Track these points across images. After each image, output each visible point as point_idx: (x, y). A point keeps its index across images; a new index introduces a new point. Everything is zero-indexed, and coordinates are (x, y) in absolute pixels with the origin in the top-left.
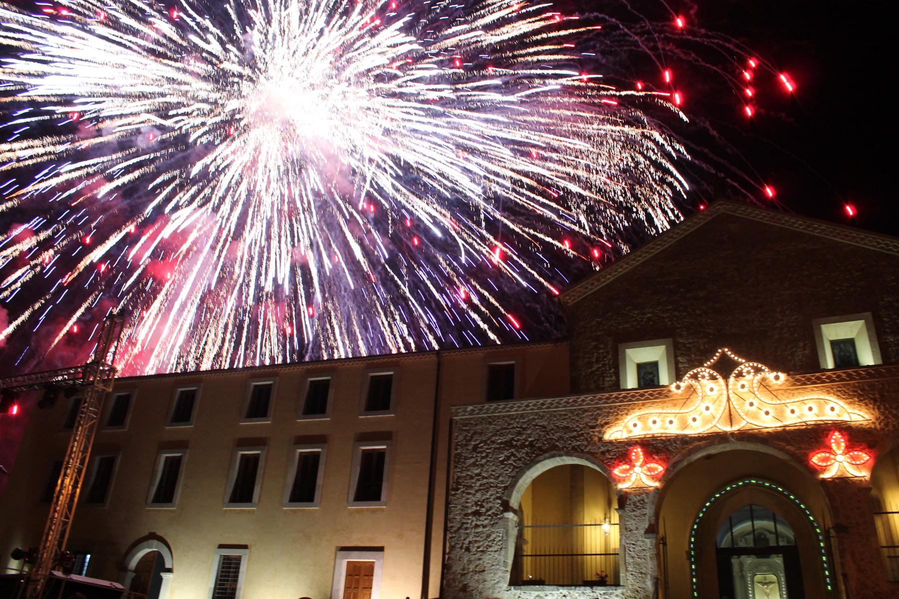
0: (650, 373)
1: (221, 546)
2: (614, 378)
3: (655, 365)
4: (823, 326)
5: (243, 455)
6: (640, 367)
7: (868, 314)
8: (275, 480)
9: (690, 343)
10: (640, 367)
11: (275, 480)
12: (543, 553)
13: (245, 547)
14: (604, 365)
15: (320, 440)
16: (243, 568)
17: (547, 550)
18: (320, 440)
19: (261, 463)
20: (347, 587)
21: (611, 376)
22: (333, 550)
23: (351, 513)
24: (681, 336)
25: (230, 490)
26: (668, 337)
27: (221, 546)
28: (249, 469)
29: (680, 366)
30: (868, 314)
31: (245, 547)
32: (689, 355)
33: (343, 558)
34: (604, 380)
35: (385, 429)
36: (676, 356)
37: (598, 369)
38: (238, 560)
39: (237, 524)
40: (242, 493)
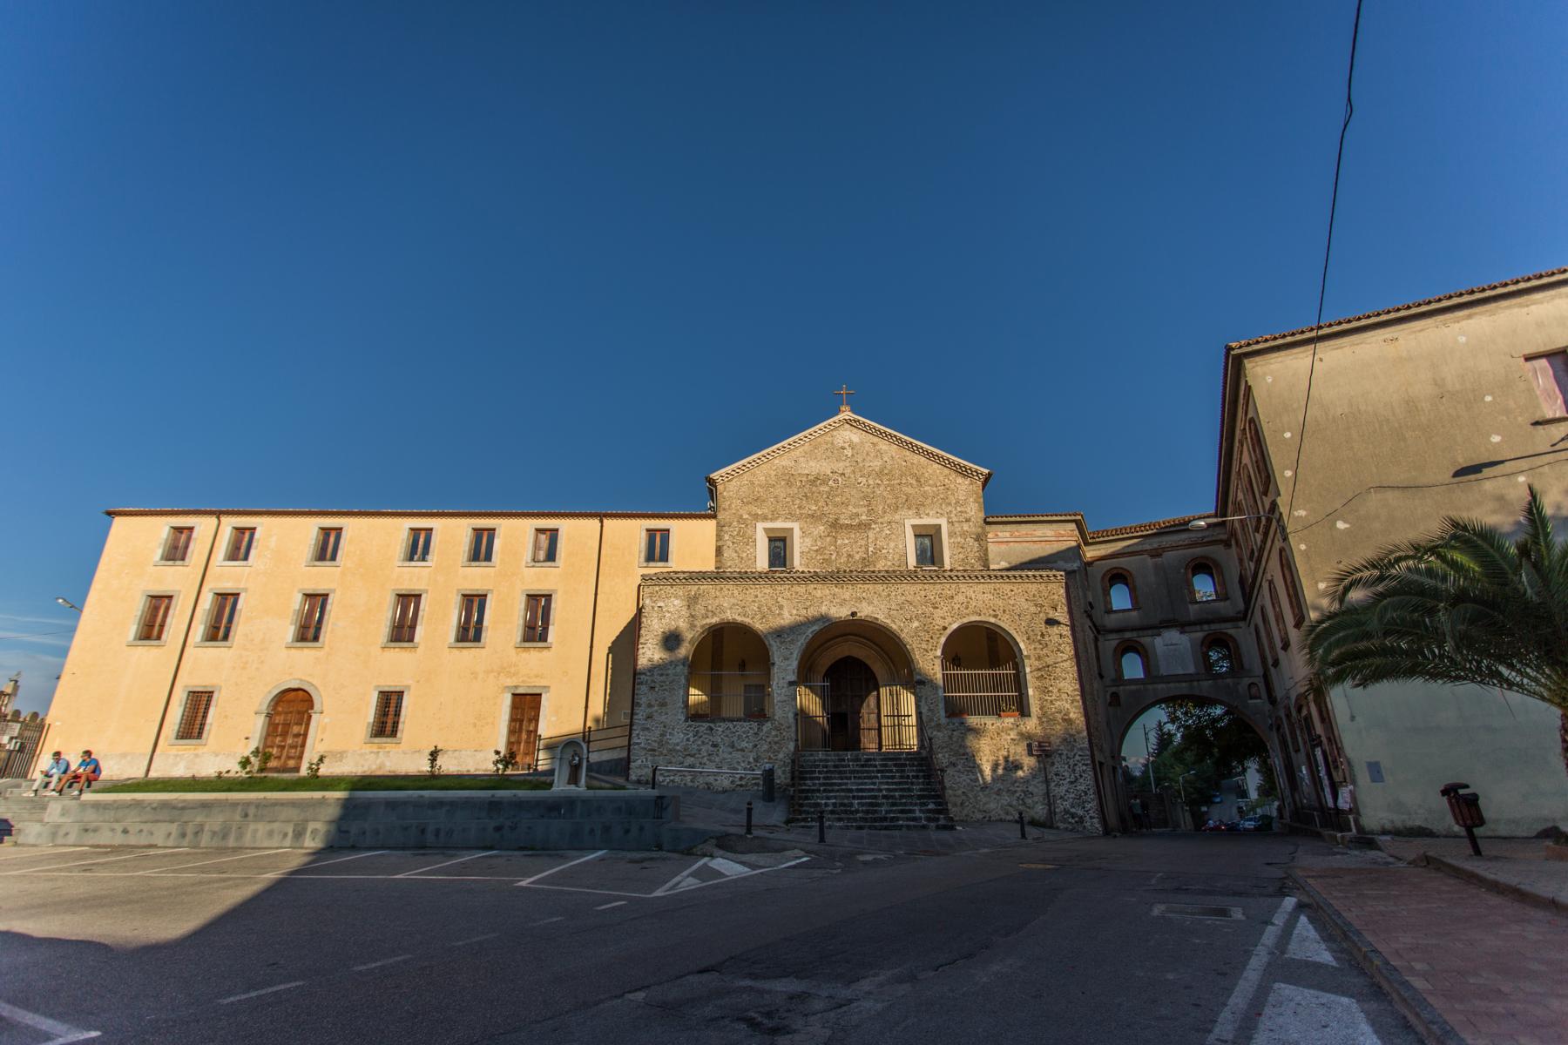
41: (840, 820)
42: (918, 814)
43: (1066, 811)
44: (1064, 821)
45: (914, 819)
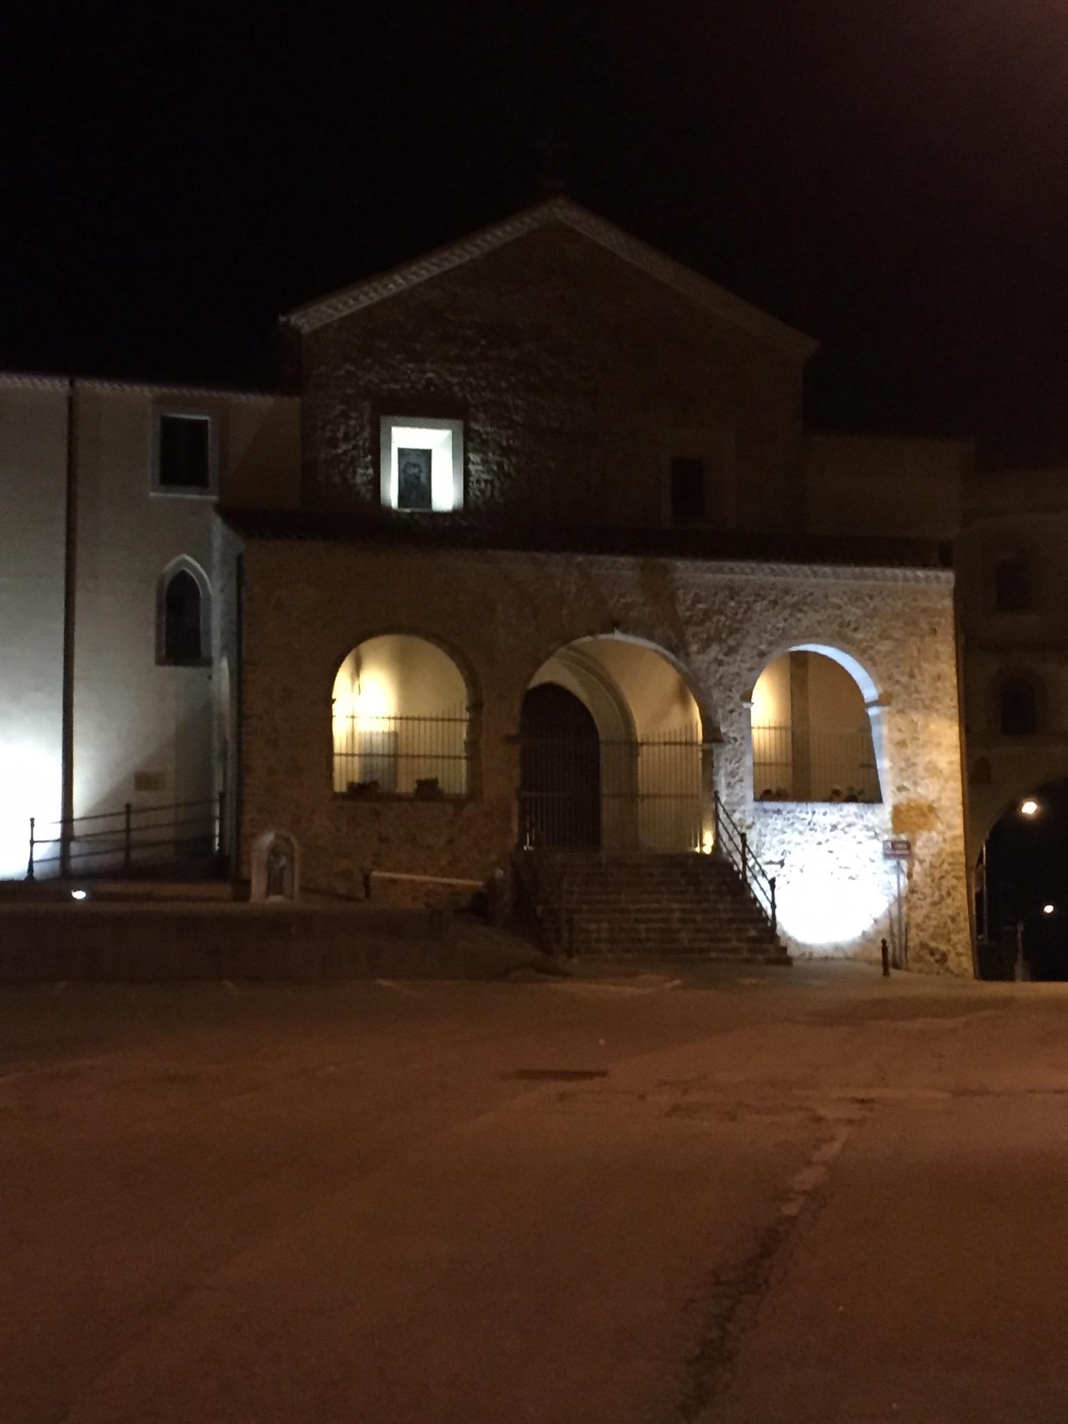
2: (371, 471)
14: (355, 447)
21: (367, 468)
24: (476, 420)
29: (471, 467)
32: (485, 453)
34: (355, 473)
36: (466, 451)
37: (345, 453)
41: (628, 950)
42: (734, 944)
43: (923, 945)
44: (919, 959)
45: (734, 950)
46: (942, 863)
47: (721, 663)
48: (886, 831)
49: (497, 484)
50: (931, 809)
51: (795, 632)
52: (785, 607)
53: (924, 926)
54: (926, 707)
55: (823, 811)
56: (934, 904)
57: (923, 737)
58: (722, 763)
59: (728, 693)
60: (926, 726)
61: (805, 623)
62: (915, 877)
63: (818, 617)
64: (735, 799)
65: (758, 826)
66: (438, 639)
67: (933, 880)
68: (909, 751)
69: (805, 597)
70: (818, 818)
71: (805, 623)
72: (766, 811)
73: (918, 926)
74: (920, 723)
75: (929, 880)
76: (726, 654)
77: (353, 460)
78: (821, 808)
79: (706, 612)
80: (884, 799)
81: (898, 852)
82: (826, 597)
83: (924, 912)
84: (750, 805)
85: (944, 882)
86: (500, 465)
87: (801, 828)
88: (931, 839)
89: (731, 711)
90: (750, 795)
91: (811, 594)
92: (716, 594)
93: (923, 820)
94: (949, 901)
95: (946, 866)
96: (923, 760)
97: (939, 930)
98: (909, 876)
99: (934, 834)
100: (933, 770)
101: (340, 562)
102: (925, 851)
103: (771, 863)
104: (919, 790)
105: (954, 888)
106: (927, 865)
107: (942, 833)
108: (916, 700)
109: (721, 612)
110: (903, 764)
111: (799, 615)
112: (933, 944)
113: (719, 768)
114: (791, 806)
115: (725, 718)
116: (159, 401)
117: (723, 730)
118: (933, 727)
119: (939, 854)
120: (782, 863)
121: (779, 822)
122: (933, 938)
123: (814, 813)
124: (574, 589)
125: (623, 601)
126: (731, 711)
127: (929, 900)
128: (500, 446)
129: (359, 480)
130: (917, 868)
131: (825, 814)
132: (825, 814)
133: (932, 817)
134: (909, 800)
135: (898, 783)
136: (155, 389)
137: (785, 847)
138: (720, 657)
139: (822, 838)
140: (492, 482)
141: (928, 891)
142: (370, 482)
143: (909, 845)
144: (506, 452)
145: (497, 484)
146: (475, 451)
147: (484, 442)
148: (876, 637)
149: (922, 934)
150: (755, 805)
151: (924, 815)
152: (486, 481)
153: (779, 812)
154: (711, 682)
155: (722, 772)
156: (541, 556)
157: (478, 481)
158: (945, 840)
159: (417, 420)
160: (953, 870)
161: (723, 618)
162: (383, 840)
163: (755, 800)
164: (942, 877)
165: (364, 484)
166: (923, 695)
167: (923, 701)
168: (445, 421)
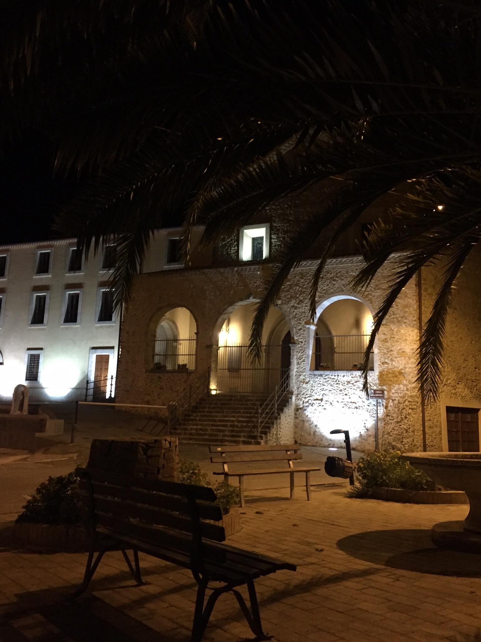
0: (260, 244)
1: (28, 349)
2: (236, 248)
3: (262, 238)
4: (245, 231)
5: (37, 296)
6: (254, 240)
7: (268, 224)
8: (56, 310)
9: (279, 226)
10: (254, 240)
11: (56, 310)
12: (351, 351)
13: (41, 349)
14: (232, 240)
15: (79, 286)
16: (41, 361)
17: (348, 349)
18: (79, 286)
19: (3, 301)
20: (97, 369)
21: (235, 247)
22: (88, 349)
23: (97, 328)
24: (275, 222)
25: (31, 317)
26: (266, 223)
27: (28, 349)
28: (41, 302)
29: (273, 240)
30: (268, 224)
31: (41, 349)
32: (278, 234)
33: (93, 354)
34: (231, 249)
35: (47, 283)
36: (271, 235)
37: (228, 243)
38: (38, 356)
39: (37, 336)
40: (38, 318)
46: (405, 401)
47: (296, 308)
48: (375, 385)
49: (283, 245)
50: (400, 373)
51: (332, 291)
52: (327, 279)
53: (391, 434)
54: (399, 322)
55: (343, 375)
56: (398, 422)
57: (397, 337)
58: (295, 353)
59: (299, 321)
60: (398, 331)
61: (337, 286)
62: (389, 408)
63: (343, 282)
64: (301, 370)
65: (311, 382)
66: (184, 307)
67: (398, 410)
68: (389, 344)
69: (337, 274)
70: (341, 378)
71: (337, 286)
72: (315, 375)
73: (388, 433)
74: (395, 330)
75: (396, 410)
76: (298, 304)
77: (230, 245)
78: (341, 373)
79: (290, 285)
80: (375, 369)
81: (377, 395)
82: (347, 272)
83: (392, 426)
84: (308, 372)
85: (404, 411)
86: (284, 238)
87: (332, 383)
88: (399, 389)
89: (300, 330)
90: (308, 368)
91: (340, 272)
92: (295, 277)
93: (396, 379)
94: (406, 421)
95: (407, 403)
96: (396, 348)
97: (398, 437)
98: (386, 407)
99: (402, 386)
100: (402, 353)
101: (210, 285)
102: (396, 395)
103: (317, 399)
104: (394, 363)
105: (409, 414)
106: (396, 402)
107: (406, 385)
108: (393, 318)
109: (297, 285)
110: (385, 351)
111: (334, 283)
112: (394, 443)
113: (293, 355)
114: (327, 373)
115: (297, 333)
116: (169, 234)
117: (296, 338)
118: (402, 331)
119: (403, 397)
120: (322, 400)
121: (322, 380)
122: (394, 441)
123: (338, 376)
124: (236, 282)
125: (255, 284)
126: (300, 330)
127: (395, 420)
128: (284, 231)
129: (232, 252)
130: (391, 403)
131: (344, 376)
132: (344, 376)
133: (401, 378)
134: (389, 369)
135: (383, 360)
136: (166, 230)
137: (324, 392)
138: (295, 305)
139: (342, 387)
140: (280, 245)
141: (395, 415)
142: (236, 252)
143: (383, 391)
144: (285, 232)
145: (283, 245)
146: (274, 234)
147: (278, 230)
148: (372, 289)
149: (390, 438)
150: (311, 372)
151: (396, 376)
152: (278, 245)
153: (321, 375)
154: (291, 317)
155: (295, 357)
156: (222, 270)
157: (275, 246)
158: (407, 389)
159: (261, 225)
160: (410, 405)
161: (298, 288)
162: (161, 388)
163: (310, 370)
164: (404, 409)
165: (234, 253)
166: (398, 316)
167: (397, 318)
168: (264, 224)
